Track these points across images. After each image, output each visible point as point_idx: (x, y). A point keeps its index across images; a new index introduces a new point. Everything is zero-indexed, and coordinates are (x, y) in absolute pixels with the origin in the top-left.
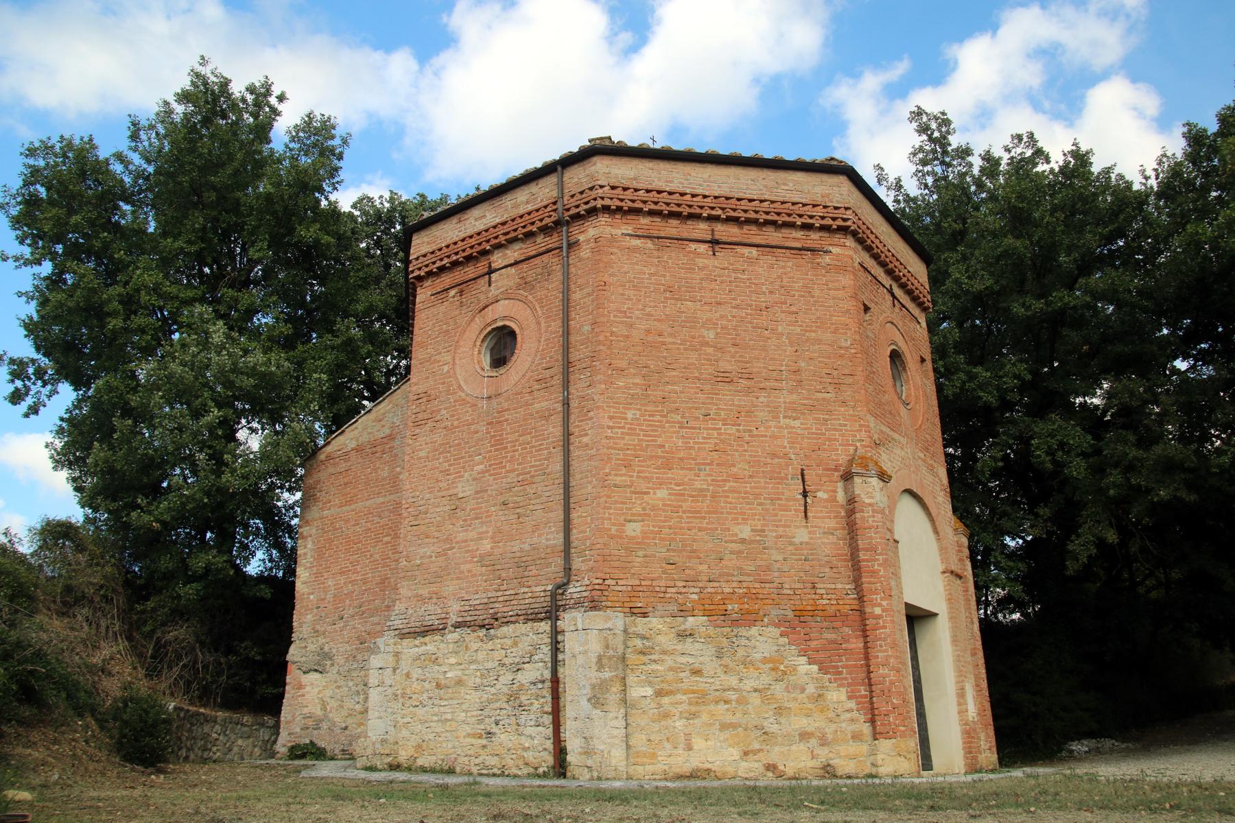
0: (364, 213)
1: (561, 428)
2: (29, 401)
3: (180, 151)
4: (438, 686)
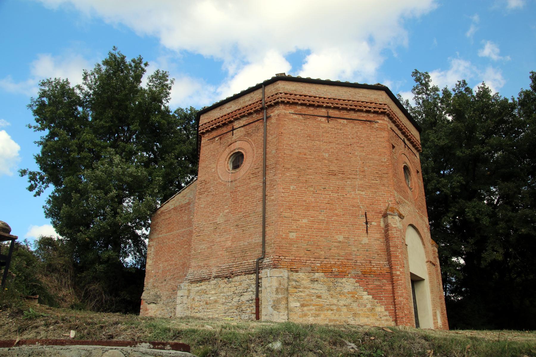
0: (179, 115)
1: (262, 193)
2: (37, 190)
3: (104, 84)
4: (207, 303)
